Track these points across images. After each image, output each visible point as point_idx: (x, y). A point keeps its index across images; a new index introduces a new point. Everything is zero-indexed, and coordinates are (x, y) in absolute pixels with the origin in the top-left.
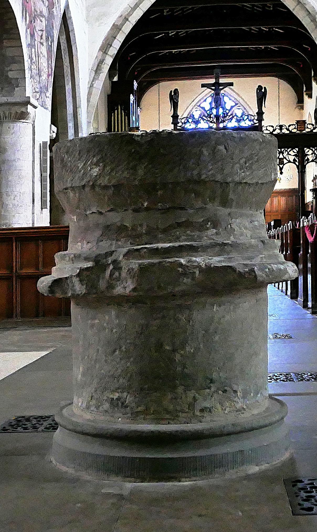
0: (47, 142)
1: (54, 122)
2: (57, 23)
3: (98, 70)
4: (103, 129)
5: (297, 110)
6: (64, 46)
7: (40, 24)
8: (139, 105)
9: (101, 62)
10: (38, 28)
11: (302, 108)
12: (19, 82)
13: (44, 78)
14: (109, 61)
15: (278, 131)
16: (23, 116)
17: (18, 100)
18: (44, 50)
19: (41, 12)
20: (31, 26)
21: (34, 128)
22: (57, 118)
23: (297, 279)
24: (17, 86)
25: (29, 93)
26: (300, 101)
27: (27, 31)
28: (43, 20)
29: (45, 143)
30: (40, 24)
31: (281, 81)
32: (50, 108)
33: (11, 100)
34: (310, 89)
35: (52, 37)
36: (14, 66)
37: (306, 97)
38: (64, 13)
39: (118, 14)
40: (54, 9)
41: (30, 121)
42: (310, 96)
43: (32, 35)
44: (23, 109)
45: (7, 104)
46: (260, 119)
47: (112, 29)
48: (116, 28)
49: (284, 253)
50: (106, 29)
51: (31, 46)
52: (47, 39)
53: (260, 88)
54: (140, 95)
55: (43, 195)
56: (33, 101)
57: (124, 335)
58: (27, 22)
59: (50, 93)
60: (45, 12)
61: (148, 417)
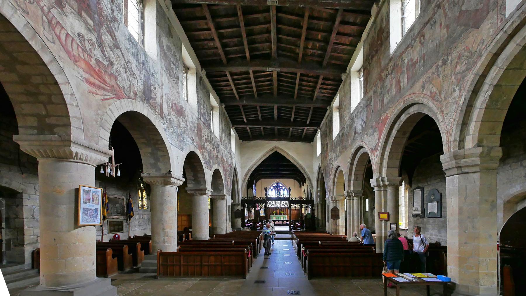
1: (232, 199)
2: (233, 171)
3: (244, 180)
4: (246, 196)
6: (235, 176)
7: (228, 173)
16: (223, 199)
18: (229, 180)
20: (225, 175)
22: (233, 197)
23: (325, 232)
26: (301, 186)
30: (228, 173)
43: (226, 177)
46: (290, 196)
48: (249, 170)
50: (246, 170)
51: (225, 180)
60: (229, 169)
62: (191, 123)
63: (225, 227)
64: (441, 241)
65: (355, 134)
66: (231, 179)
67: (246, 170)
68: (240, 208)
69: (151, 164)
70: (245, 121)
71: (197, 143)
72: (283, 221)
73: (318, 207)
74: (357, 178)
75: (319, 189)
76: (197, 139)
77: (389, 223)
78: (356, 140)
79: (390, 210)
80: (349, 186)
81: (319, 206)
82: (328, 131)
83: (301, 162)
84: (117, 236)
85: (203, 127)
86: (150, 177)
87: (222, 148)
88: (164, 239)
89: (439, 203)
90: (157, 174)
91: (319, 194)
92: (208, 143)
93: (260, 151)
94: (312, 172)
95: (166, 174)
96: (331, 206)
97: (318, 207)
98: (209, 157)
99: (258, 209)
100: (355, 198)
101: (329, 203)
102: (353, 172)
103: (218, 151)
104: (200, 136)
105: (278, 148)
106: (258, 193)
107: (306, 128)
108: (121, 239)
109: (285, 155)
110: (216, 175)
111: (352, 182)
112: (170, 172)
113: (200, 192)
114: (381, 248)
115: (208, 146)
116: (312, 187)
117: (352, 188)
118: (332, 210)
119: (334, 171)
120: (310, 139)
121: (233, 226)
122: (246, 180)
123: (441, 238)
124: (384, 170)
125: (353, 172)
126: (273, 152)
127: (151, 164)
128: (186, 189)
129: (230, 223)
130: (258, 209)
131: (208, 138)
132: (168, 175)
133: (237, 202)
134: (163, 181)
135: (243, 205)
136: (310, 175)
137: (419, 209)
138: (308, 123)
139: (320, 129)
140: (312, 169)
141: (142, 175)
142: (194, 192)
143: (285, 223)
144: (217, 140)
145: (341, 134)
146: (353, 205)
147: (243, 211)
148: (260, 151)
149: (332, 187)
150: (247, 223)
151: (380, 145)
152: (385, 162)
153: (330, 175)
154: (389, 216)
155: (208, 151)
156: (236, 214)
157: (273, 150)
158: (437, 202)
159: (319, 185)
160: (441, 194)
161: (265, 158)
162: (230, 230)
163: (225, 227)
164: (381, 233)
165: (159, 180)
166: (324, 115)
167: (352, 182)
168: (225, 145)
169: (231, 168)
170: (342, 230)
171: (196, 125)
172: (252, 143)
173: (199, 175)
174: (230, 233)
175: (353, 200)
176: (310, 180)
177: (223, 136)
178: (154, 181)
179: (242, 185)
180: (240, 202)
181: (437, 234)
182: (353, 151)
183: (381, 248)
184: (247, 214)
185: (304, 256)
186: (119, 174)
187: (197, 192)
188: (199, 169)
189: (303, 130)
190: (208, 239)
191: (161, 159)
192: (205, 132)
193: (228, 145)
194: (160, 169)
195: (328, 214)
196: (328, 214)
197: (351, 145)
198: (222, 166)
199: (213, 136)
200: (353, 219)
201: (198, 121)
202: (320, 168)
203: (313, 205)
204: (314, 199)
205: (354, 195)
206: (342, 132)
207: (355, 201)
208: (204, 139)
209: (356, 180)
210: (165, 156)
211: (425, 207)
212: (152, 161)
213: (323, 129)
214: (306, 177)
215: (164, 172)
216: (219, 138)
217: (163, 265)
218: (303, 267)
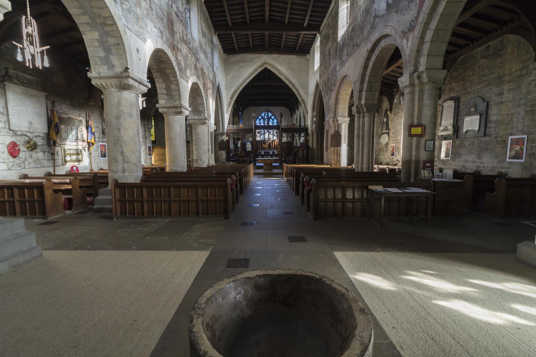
34: (295, 111)
48: (235, 92)
50: (234, 89)
60: (211, 87)
62: (157, 7)
63: (206, 158)
64: (482, 168)
65: (374, 20)
69: (101, 58)
70: (230, 24)
71: (167, 38)
73: (313, 135)
74: (371, 87)
75: (315, 114)
76: (168, 34)
77: (423, 140)
78: (375, 28)
79: (426, 120)
80: (360, 99)
81: (315, 134)
82: (331, 33)
83: (294, 81)
84: (75, 168)
85: (176, 20)
86: (100, 78)
87: (202, 56)
88: (123, 167)
89: (484, 117)
90: (110, 73)
91: (315, 119)
92: (183, 45)
93: (248, 68)
94: (307, 93)
95: (122, 73)
96: (332, 131)
97: (313, 135)
98: (185, 64)
100: (366, 114)
101: (329, 128)
102: (367, 78)
103: (197, 60)
104: (172, 32)
107: (303, 33)
108: (80, 171)
109: (276, 72)
110: (195, 91)
111: (364, 93)
112: (127, 69)
113: (174, 110)
115: (184, 49)
116: (307, 112)
117: (363, 102)
118: (332, 136)
119: (338, 84)
120: (305, 50)
121: (216, 160)
123: (482, 165)
124: (423, 61)
125: (367, 78)
126: (262, 68)
127: (101, 58)
128: (157, 106)
129: (213, 155)
131: (183, 38)
132: (125, 74)
133: (221, 131)
134: (118, 83)
136: (304, 97)
137: (450, 127)
138: (305, 25)
139: (320, 34)
140: (308, 89)
141: (89, 75)
142: (166, 110)
144: (196, 44)
145: (350, 29)
146: (363, 125)
148: (248, 68)
149: (334, 106)
150: (233, 157)
151: (420, 20)
152: (426, 48)
153: (332, 91)
154: (424, 131)
155: (183, 56)
157: (262, 66)
158: (481, 115)
159: (315, 109)
160: (488, 103)
162: (213, 163)
163: (206, 158)
164: (411, 155)
165: (114, 81)
166: (326, 13)
167: (364, 93)
168: (205, 54)
171: (166, 13)
172: (238, 57)
173: (173, 87)
174: (213, 166)
175: (364, 117)
177: (203, 41)
178: (106, 84)
181: (475, 159)
182: (369, 46)
185: (307, 188)
186: (47, 64)
187: (171, 110)
188: (172, 79)
189: (298, 36)
190: (185, 171)
191: (114, 51)
192: (178, 28)
193: (209, 55)
194: (113, 66)
195: (327, 142)
196: (327, 142)
197: (368, 38)
199: (189, 37)
200: (363, 144)
201: (168, 8)
202: (317, 86)
203: (307, 135)
205: (365, 110)
206: (353, 25)
207: (366, 119)
208: (177, 36)
209: (369, 90)
210: (118, 44)
211: (459, 124)
212: (102, 54)
213: (324, 33)
215: (119, 69)
216: (197, 41)
217: (119, 200)
218: (303, 203)
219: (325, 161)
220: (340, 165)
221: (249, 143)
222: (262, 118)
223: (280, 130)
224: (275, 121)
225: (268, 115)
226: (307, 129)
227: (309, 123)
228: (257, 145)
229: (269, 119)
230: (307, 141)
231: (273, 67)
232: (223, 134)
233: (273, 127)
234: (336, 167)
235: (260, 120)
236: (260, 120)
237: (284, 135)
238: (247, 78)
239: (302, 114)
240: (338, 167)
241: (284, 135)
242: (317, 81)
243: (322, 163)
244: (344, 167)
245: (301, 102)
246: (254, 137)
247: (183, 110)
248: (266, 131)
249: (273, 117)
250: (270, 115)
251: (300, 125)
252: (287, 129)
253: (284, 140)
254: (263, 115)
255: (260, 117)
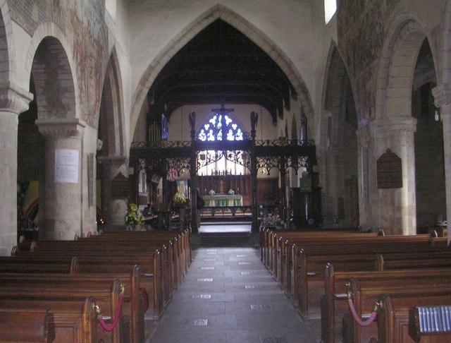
0: (93, 154)
1: (100, 137)
2: (105, 62)
5: (272, 126)
8: (168, 121)
9: (141, 91)
10: (87, 66)
11: (276, 125)
12: (69, 108)
13: (92, 103)
14: (146, 91)
15: (265, 144)
16: (73, 133)
17: (70, 121)
18: (93, 82)
19: (91, 53)
21: (82, 142)
24: (69, 110)
25: (78, 115)
26: (275, 121)
27: (77, 68)
28: (93, 60)
29: (92, 155)
31: (263, 108)
32: (97, 126)
33: (63, 120)
34: (281, 113)
35: (100, 73)
36: (68, 95)
37: (278, 119)
38: (112, 54)
39: (152, 59)
40: (103, 53)
41: (80, 137)
42: (282, 118)
43: (83, 71)
44: (73, 128)
45: (59, 124)
47: (148, 69)
48: (151, 68)
49: (339, 319)
50: (148, 63)
52: (96, 74)
53: (253, 113)
54: (168, 116)
55: (90, 195)
56: (82, 122)
57: (151, 167)
58: (79, 60)
59: (97, 115)
60: (95, 54)
61: (164, 305)
66: (98, 83)
67: (143, 69)
68: (125, 170)
72: (234, 209)
83: (281, 45)
99: (171, 176)
105: (225, 10)
106: (174, 134)
114: (447, 327)
116: (311, 110)
122: (144, 96)
126: (211, 20)
130: (171, 176)
133: (118, 153)
135: (134, 162)
143: (239, 213)
147: (134, 179)
156: (108, 183)
157: (211, 15)
161: (191, 36)
169: (99, 55)
170: (410, 222)
176: (305, 92)
179: (133, 109)
180: (127, 153)
183: (447, 327)
184: (142, 189)
198: (71, 36)
204: (317, 143)
214: (295, 84)
219: (363, 220)
220: (401, 231)
221: (182, 182)
222: (211, 127)
223: (251, 149)
224: (239, 133)
225: (223, 121)
226: (313, 148)
227: (318, 137)
228: (201, 185)
229: (225, 129)
230: (312, 176)
231: (237, 16)
232: (121, 161)
233: (235, 146)
234: (389, 236)
235: (207, 132)
236: (207, 132)
237: (261, 162)
238: (179, 40)
239: (298, 116)
240: (396, 236)
241: (261, 162)
242: (333, 43)
243: (356, 229)
244: (409, 238)
245: (298, 90)
246: (193, 168)
247: (12, 97)
248: (220, 152)
249: (235, 126)
250: (228, 120)
251: (295, 140)
252: (268, 148)
253: (263, 172)
254: (213, 121)
255: (207, 127)
